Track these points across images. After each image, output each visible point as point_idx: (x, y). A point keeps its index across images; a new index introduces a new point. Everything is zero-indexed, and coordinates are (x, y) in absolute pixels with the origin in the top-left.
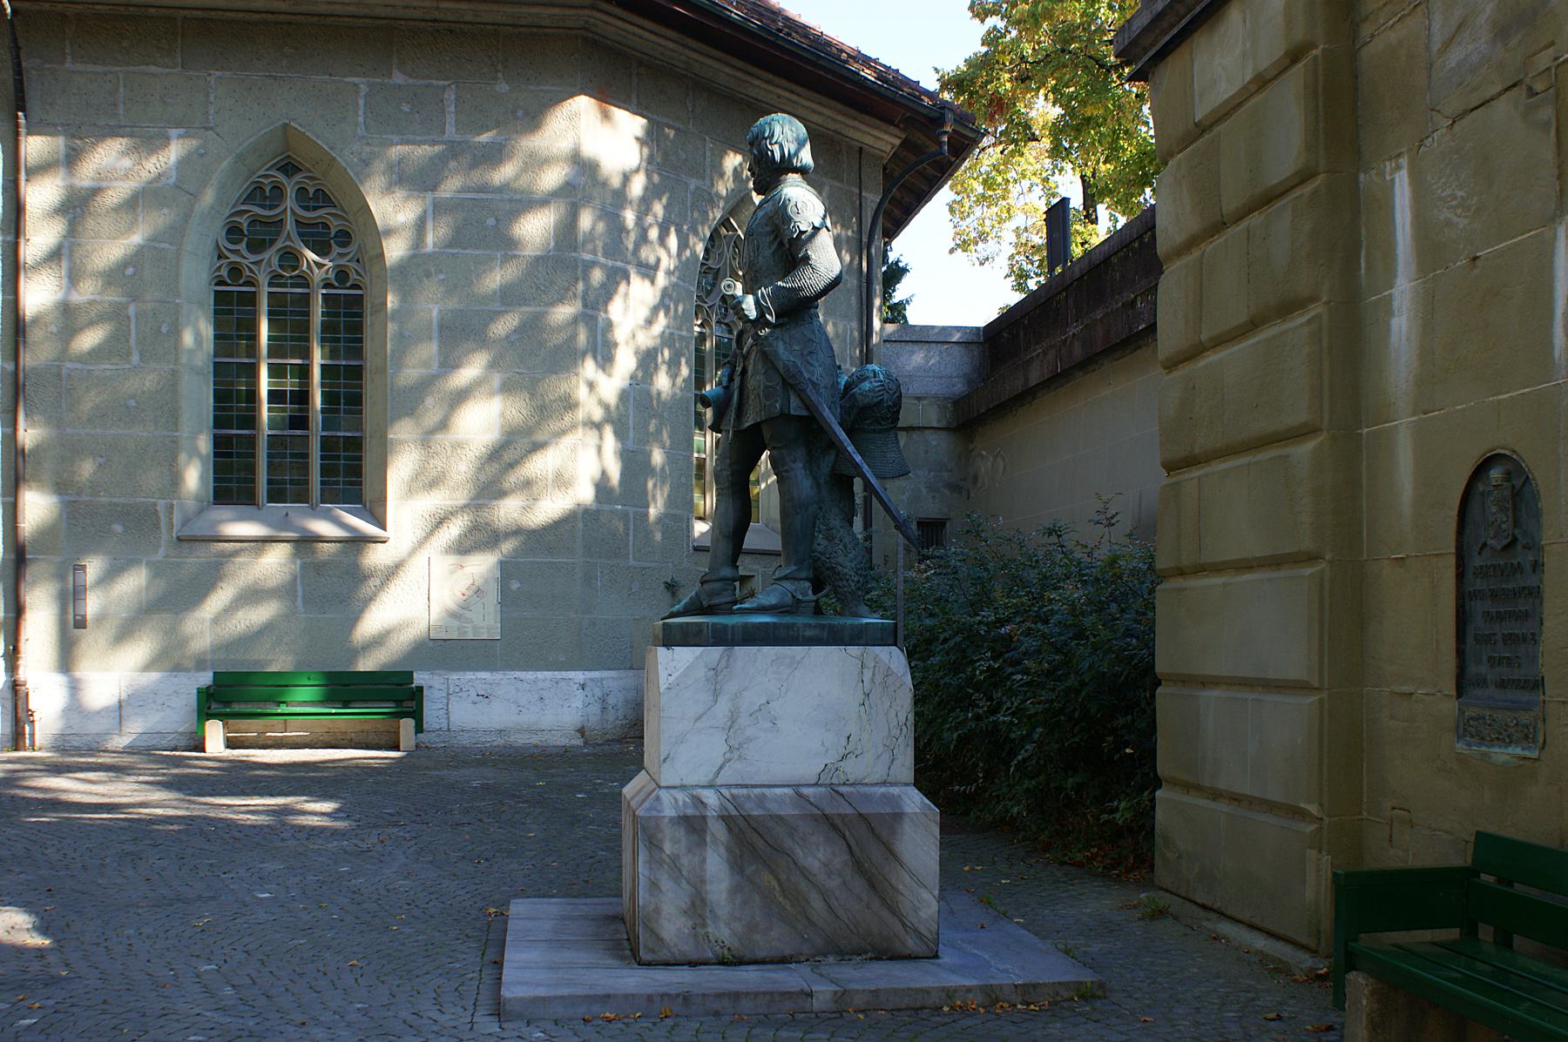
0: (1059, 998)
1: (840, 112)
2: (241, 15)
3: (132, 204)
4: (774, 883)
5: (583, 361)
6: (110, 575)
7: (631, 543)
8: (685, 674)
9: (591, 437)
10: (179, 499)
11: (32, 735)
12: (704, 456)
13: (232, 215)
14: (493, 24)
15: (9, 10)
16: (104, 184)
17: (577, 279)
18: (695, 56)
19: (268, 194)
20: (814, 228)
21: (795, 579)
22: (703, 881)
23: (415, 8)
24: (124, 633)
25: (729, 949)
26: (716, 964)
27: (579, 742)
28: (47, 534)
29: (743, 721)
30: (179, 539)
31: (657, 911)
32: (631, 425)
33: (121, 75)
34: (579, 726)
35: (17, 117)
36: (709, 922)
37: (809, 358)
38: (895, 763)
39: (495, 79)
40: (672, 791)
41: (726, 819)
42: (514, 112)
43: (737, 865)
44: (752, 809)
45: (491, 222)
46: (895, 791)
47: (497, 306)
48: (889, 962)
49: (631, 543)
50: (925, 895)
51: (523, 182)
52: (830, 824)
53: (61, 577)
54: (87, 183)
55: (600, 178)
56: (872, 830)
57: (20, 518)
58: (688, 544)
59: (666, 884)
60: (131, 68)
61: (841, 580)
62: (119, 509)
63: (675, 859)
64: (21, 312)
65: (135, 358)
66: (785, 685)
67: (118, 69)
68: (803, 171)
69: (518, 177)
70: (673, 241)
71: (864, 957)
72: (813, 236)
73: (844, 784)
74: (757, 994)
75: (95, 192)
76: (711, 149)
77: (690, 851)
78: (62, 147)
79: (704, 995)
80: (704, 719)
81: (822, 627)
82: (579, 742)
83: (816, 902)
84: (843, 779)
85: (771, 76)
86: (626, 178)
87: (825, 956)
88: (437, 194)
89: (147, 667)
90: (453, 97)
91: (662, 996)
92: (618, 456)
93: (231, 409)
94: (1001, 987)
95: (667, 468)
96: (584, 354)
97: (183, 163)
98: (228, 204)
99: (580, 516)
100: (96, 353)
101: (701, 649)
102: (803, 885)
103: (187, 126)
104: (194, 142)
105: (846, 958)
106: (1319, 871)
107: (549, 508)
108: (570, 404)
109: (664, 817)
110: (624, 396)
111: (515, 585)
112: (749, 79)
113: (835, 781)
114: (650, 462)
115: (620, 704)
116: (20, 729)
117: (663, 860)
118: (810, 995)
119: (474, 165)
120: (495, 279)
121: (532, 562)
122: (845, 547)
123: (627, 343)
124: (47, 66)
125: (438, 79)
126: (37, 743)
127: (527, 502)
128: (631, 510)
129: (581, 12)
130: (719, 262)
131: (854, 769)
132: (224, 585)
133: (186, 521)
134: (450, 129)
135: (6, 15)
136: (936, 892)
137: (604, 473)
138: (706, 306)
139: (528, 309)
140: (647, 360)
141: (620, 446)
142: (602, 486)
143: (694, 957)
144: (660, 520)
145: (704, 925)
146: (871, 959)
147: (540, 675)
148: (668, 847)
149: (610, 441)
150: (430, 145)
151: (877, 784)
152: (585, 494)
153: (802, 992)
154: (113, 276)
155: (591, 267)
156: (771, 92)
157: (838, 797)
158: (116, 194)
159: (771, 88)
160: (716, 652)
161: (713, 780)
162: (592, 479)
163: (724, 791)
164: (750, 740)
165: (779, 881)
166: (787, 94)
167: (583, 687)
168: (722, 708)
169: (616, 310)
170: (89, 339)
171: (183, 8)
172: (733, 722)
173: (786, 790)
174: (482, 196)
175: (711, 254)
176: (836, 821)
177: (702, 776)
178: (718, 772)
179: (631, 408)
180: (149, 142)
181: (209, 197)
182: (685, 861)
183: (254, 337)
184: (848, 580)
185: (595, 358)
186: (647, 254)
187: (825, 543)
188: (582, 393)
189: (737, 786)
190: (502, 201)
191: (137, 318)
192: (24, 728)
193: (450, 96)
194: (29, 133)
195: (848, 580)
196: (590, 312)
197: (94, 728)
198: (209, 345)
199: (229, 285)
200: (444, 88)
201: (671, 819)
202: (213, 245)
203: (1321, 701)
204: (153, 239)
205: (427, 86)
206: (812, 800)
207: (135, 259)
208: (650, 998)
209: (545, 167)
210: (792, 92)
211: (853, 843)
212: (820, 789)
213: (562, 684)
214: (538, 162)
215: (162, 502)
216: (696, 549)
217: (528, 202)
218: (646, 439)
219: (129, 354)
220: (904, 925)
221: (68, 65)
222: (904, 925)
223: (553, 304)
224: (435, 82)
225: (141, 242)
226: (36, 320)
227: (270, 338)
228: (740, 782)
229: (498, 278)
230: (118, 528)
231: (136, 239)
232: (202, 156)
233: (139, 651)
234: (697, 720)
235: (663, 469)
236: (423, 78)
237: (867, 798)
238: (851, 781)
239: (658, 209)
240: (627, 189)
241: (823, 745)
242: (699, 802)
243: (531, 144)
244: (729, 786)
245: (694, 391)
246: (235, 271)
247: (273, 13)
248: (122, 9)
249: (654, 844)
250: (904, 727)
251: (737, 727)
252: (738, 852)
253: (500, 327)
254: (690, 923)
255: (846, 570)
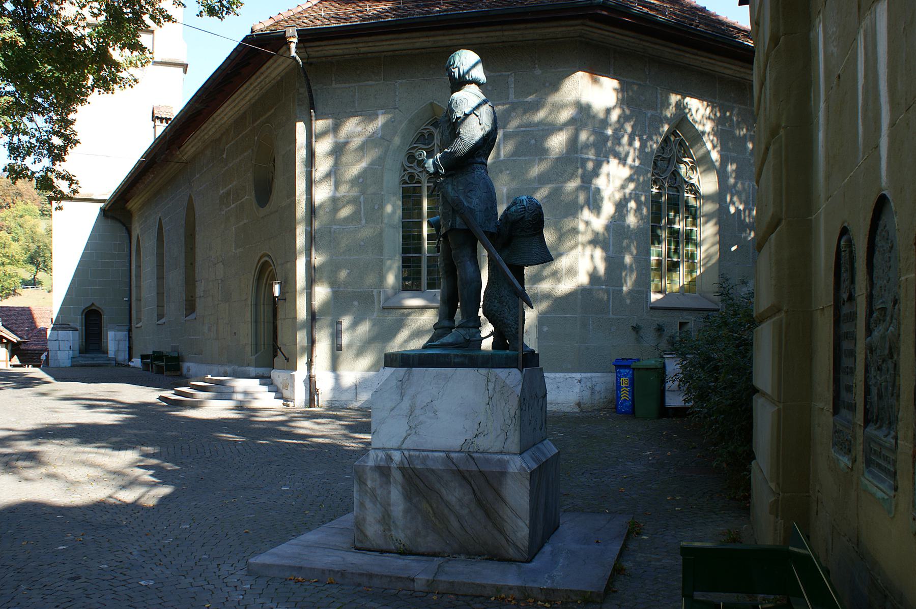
0: (570, 600)
1: (742, 67)
2: (410, 52)
3: (362, 148)
4: (430, 509)
5: (582, 211)
6: (354, 325)
7: (611, 306)
8: (385, 384)
9: (589, 250)
10: (383, 288)
11: (318, 400)
12: (661, 258)
13: (409, 150)
14: (532, 40)
15: (301, 63)
16: (350, 140)
17: (578, 168)
18: (647, 44)
19: (426, 138)
20: (465, 114)
21: (467, 327)
22: (389, 505)
23: (492, 37)
24: (360, 352)
25: (403, 545)
26: (396, 553)
27: (577, 410)
28: (326, 305)
29: (417, 412)
30: (383, 308)
31: (364, 519)
32: (611, 243)
33: (356, 87)
34: (578, 401)
35: (311, 112)
36: (392, 528)
37: (469, 194)
38: (508, 440)
39: (534, 68)
40: (377, 451)
41: (401, 469)
42: (544, 84)
43: (408, 497)
44: (417, 464)
45: (533, 142)
46: (506, 457)
47: (536, 185)
48: (497, 562)
49: (611, 306)
50: (521, 524)
51: (550, 119)
52: (463, 476)
53: (331, 325)
54: (342, 140)
55: (592, 114)
56: (488, 481)
57: (313, 299)
58: (647, 306)
59: (369, 505)
60: (361, 84)
61: (507, 327)
62: (356, 294)
63: (373, 490)
64: (313, 203)
65: (364, 222)
66: (442, 391)
67: (355, 84)
68: (475, 82)
69: (546, 117)
70: (637, 144)
71: (483, 557)
72: (464, 120)
73: (477, 452)
74: (382, 576)
75: (346, 143)
76: (661, 94)
77: (381, 486)
78: (331, 124)
79: (352, 573)
80: (395, 410)
81: (465, 356)
82: (577, 410)
83: (454, 523)
84: (476, 448)
85: (695, 51)
86: (608, 111)
87: (459, 554)
88: (505, 130)
89: (369, 370)
90: (513, 80)
91: (330, 571)
92: (603, 260)
93: (410, 244)
94: (531, 588)
95: (634, 266)
96: (582, 208)
97: (385, 125)
98: (407, 144)
99: (580, 292)
100: (347, 220)
101: (394, 369)
102: (446, 511)
103: (386, 108)
104: (390, 116)
105: (472, 557)
106: (776, 530)
107: (565, 287)
108: (575, 231)
109: (367, 466)
110: (607, 228)
111: (545, 329)
112: (681, 53)
113: (471, 450)
114: (623, 262)
115: (603, 390)
116: (312, 398)
117: (367, 491)
118: (413, 580)
119: (524, 113)
120: (535, 171)
121: (554, 317)
122: (509, 307)
123: (610, 198)
124: (325, 87)
125: (505, 71)
126: (320, 405)
127: (552, 286)
128: (611, 288)
129: (576, 28)
130: (670, 153)
131: (483, 443)
132: (404, 330)
133: (387, 299)
134: (512, 96)
135: (300, 65)
136: (528, 522)
137: (595, 268)
138: (661, 178)
139: (554, 185)
140: (621, 206)
141: (604, 254)
142: (593, 276)
143: (384, 547)
144: (630, 292)
145: (390, 530)
146: (487, 559)
147: (558, 375)
148: (369, 483)
149: (599, 253)
150: (502, 106)
151: (496, 453)
152: (583, 279)
153: (408, 578)
154: (354, 182)
155: (586, 161)
156: (697, 60)
157: (470, 460)
158: (356, 142)
159: (698, 58)
160: (402, 371)
161: (401, 446)
162: (588, 272)
163: (406, 453)
164: (421, 423)
165: (432, 507)
166: (707, 60)
167: (580, 381)
168: (406, 404)
169: (600, 182)
170: (345, 212)
171: (383, 52)
172: (412, 412)
173: (441, 454)
174: (528, 129)
175: (665, 151)
176: (465, 474)
177: (394, 443)
178: (403, 442)
179: (611, 234)
180: (370, 116)
181: (397, 140)
182: (379, 492)
183: (421, 209)
184: (510, 328)
185: (589, 209)
186: (622, 150)
187: (497, 305)
188: (582, 227)
189: (414, 450)
190: (538, 130)
191: (364, 202)
192: (314, 397)
193: (511, 79)
194: (316, 120)
195: (510, 328)
196: (586, 185)
197: (344, 397)
198: (399, 212)
199: (408, 184)
200: (508, 76)
201: (371, 467)
202: (401, 164)
203: (779, 410)
204: (372, 164)
205: (500, 76)
206: (454, 461)
207: (363, 174)
208: (323, 571)
209: (560, 111)
210: (710, 58)
211: (475, 488)
212: (462, 454)
213: (569, 380)
214: (560, 107)
215: (375, 291)
216: (652, 308)
217: (552, 128)
218: (622, 251)
219: (361, 220)
220: (507, 540)
221: (334, 85)
222: (507, 540)
223: (565, 182)
224: (504, 73)
225: (366, 166)
226: (321, 206)
227: (428, 208)
228: (416, 448)
229: (537, 170)
230: (356, 303)
231: (363, 164)
232: (393, 122)
233: (366, 361)
234: (391, 411)
235: (631, 266)
236: (499, 72)
237: (488, 461)
238: (481, 450)
239: (628, 128)
240: (609, 118)
241: (464, 428)
242: (389, 458)
243: (553, 100)
244: (409, 450)
245: (651, 224)
246: (411, 177)
247: (424, 49)
248: (356, 56)
249: (362, 482)
250: (513, 419)
251: (414, 415)
252: (409, 489)
253: (538, 196)
254: (382, 528)
255: (509, 322)
